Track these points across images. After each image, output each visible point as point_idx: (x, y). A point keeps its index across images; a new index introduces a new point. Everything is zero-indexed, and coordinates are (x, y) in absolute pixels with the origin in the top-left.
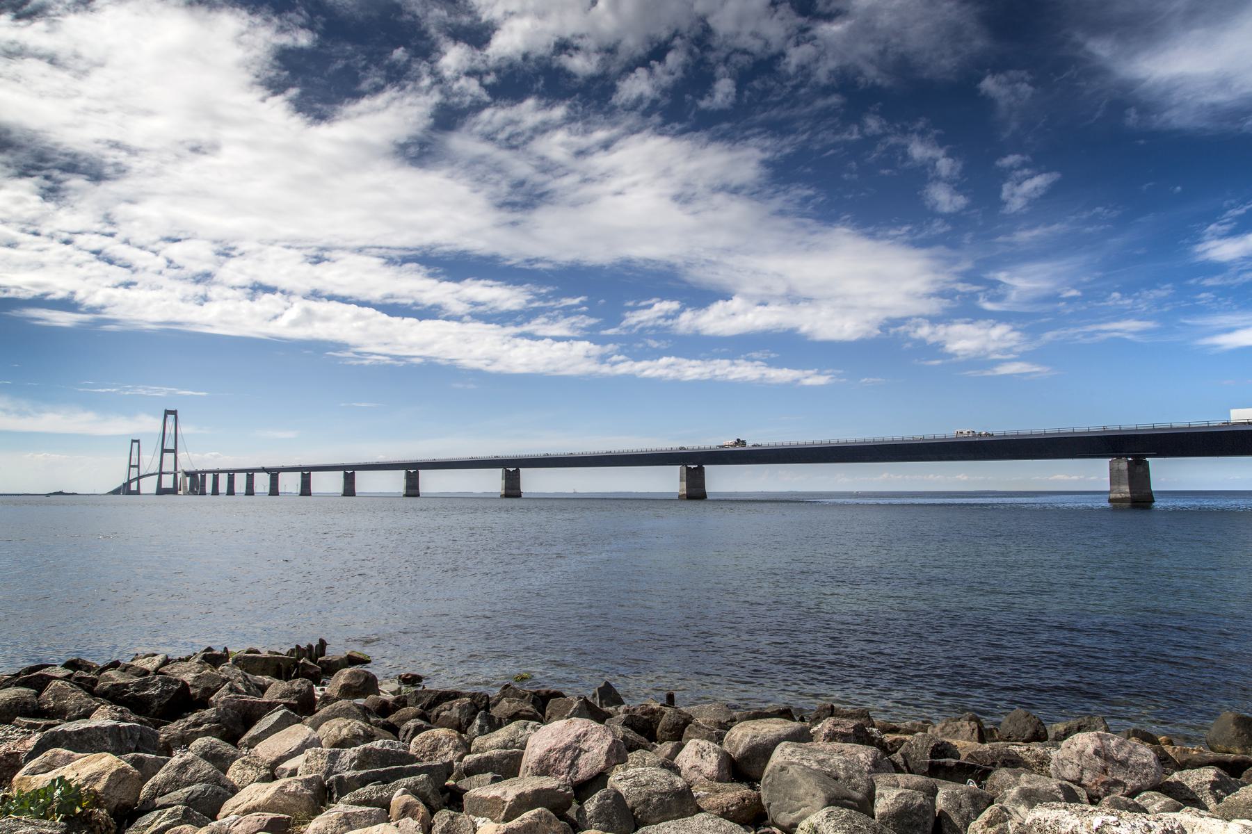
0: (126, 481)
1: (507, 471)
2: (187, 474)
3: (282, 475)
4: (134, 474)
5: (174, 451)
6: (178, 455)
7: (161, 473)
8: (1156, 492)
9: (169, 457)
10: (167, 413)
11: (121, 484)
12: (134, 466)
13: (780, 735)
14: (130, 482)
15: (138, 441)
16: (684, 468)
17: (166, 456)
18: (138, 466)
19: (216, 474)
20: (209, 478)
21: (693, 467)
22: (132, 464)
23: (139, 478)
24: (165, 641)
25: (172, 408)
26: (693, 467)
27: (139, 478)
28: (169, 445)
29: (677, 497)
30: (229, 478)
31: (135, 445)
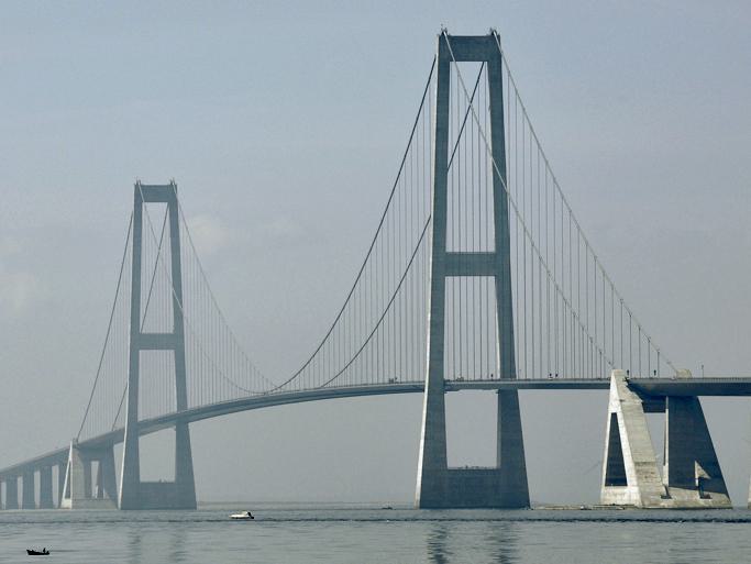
4: (159, 399)
7: (440, 387)
9: (471, 296)
18: (174, 341)
23: (182, 420)
27: (182, 420)
28: (471, 233)
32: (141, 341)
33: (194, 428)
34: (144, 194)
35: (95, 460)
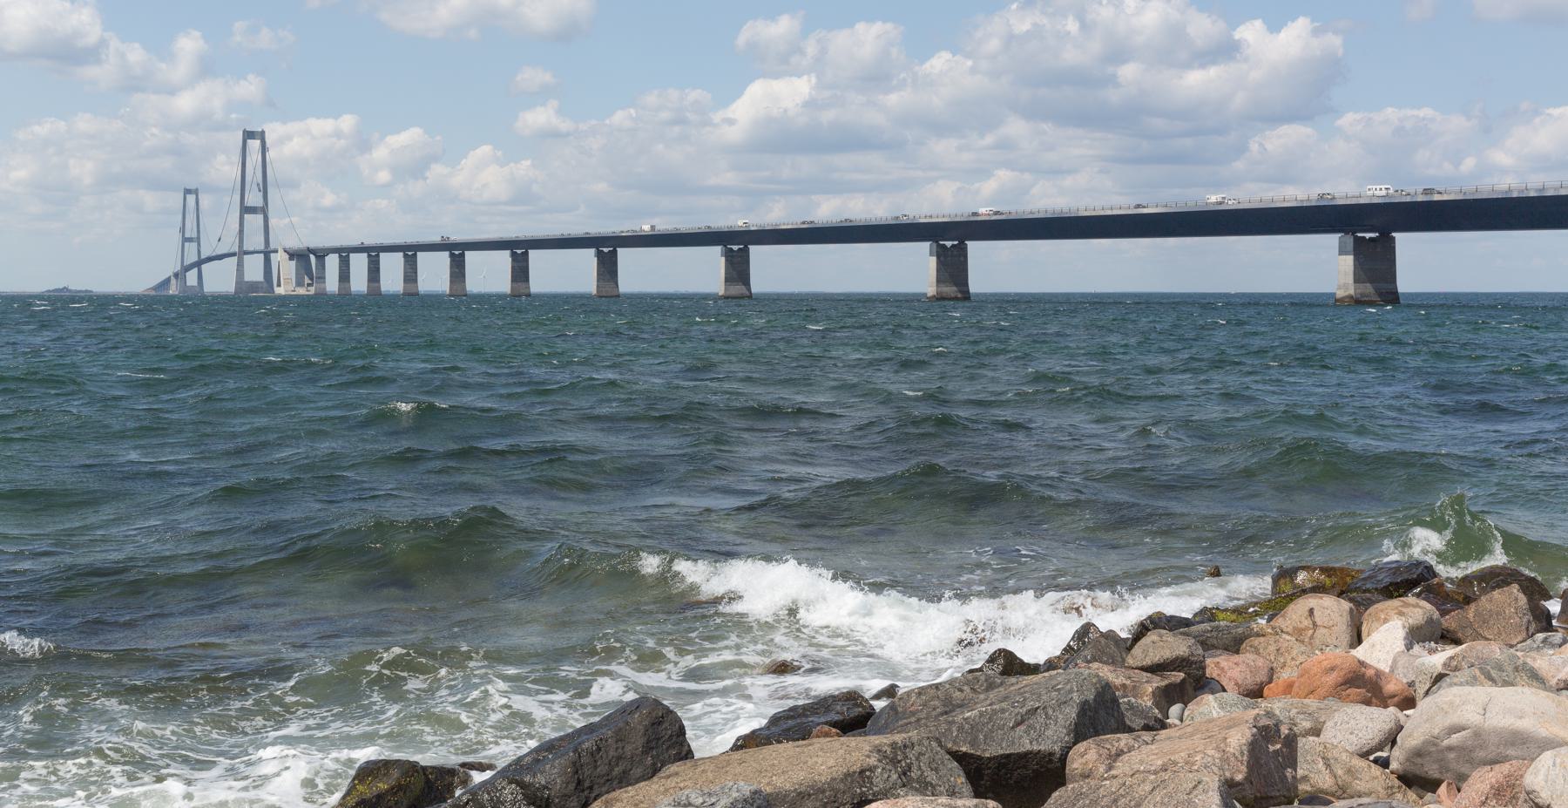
0: (178, 268)
1: (939, 245)
2: (292, 255)
3: (422, 257)
4: (192, 258)
6: (272, 222)
7: (242, 253)
8: (1403, 294)
9: (253, 221)
10: (249, 135)
12: (190, 240)
13: (904, 593)
15: (196, 192)
16: (1350, 240)
17: (587, 259)
19: (344, 253)
20: (332, 262)
21: (1368, 235)
23: (198, 264)
24: (296, 617)
25: (193, 187)
26: (1368, 235)
27: (198, 264)
29: (1332, 301)
30: (370, 263)
31: (254, 144)
33: (204, 267)
35: (360, 296)
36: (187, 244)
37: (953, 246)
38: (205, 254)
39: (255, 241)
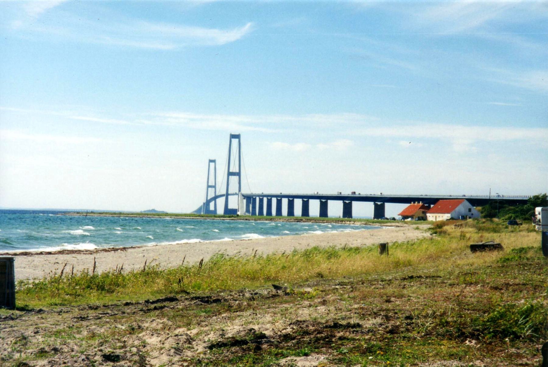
0: (205, 201)
4: (211, 195)
5: (238, 174)
9: (234, 179)
11: (202, 204)
14: (208, 202)
18: (214, 187)
22: (210, 184)
23: (215, 198)
27: (215, 198)
32: (209, 186)
33: (218, 200)
34: (211, 161)
36: (214, 184)
37: (381, 204)
38: (218, 194)
39: (234, 188)
